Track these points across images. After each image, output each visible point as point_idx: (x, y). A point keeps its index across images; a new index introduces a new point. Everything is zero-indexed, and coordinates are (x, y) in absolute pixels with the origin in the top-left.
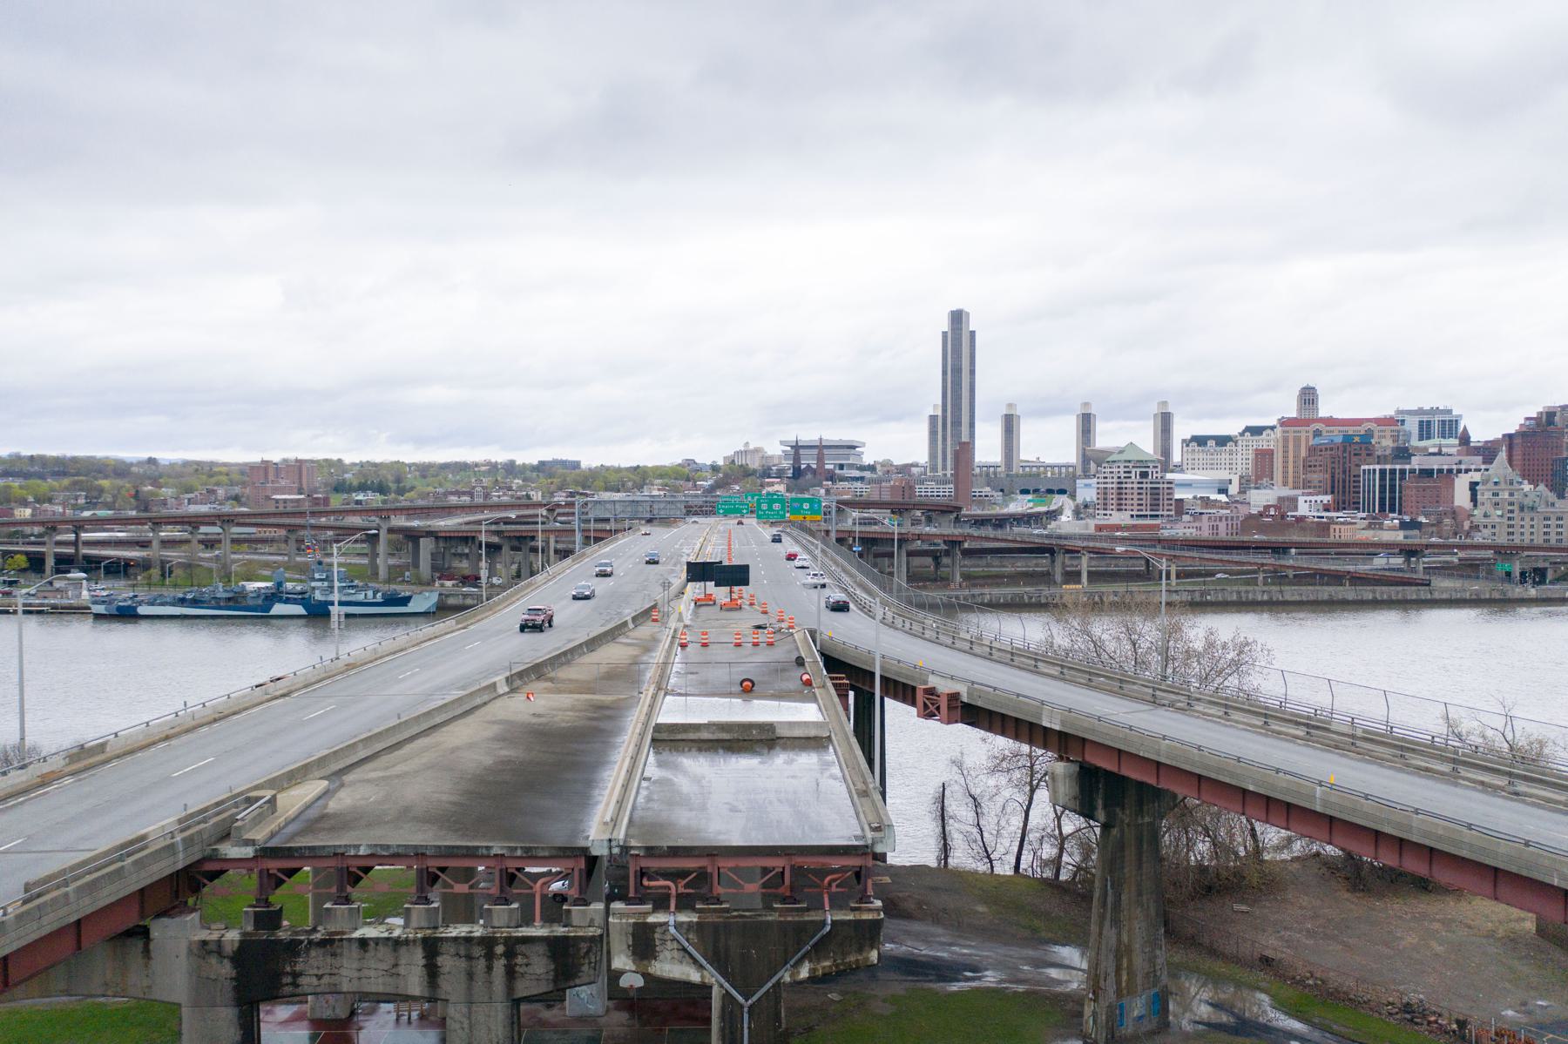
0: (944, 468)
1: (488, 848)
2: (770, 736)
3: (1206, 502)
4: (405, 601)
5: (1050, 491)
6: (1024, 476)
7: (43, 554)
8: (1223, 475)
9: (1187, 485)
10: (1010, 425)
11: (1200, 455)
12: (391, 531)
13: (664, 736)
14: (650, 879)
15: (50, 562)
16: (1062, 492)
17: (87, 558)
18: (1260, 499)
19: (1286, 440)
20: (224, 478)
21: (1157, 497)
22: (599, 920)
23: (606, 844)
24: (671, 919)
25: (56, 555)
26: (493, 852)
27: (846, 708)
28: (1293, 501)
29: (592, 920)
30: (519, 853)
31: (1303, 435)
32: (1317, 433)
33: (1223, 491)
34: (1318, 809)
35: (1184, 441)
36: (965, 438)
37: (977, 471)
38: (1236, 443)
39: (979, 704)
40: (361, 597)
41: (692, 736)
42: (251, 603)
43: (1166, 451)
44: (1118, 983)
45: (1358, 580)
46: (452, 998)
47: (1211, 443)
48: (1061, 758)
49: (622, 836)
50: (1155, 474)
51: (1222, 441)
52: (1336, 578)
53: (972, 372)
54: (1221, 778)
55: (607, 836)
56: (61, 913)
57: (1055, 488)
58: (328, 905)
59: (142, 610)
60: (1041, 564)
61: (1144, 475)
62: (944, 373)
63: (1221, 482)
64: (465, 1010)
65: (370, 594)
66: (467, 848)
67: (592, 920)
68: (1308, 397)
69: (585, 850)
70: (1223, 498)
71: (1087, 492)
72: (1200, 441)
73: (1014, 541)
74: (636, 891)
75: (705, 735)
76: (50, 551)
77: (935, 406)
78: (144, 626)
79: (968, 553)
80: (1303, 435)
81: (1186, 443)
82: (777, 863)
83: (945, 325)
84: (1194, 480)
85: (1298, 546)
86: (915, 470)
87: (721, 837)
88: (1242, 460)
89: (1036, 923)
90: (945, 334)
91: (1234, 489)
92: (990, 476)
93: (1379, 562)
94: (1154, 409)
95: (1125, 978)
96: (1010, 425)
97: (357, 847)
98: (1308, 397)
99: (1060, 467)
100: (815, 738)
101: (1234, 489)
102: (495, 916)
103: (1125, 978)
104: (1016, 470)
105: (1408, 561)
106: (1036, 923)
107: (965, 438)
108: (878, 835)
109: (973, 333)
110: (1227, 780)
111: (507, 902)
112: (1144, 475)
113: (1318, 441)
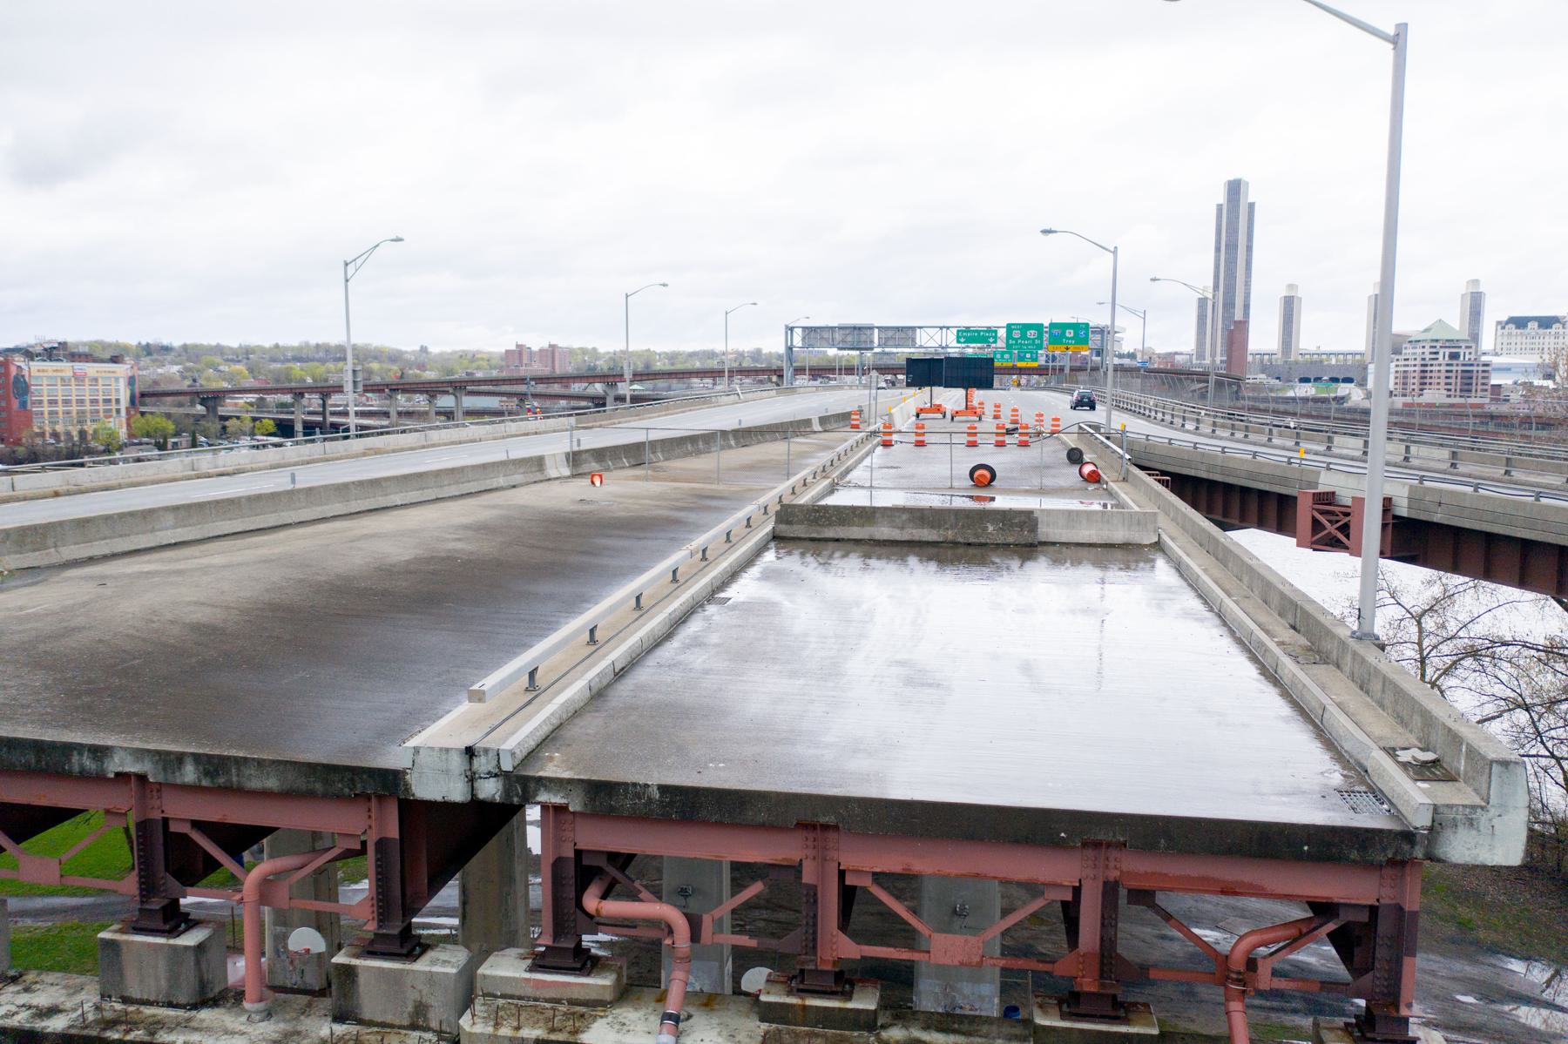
0: (1213, 355)
1: (99, 752)
2: (1026, 536)
3: (1528, 386)
5: (1334, 380)
6: (1306, 363)
7: (292, 421)
9: (1506, 369)
10: (1289, 308)
13: (799, 530)
15: (299, 427)
16: (1349, 380)
20: (485, 364)
21: (1468, 380)
23: (457, 763)
26: (114, 765)
29: (421, 1009)
30: (189, 774)
33: (1549, 376)
35: (1499, 323)
36: (1238, 316)
37: (1250, 358)
39: (1438, 517)
41: (856, 532)
43: (1475, 337)
47: (1533, 325)
50: (1466, 355)
53: (1249, 248)
61: (1454, 356)
62: (1218, 249)
66: (38, 746)
67: (421, 1009)
69: (389, 783)
70: (1550, 384)
72: (1520, 323)
75: (884, 532)
76: (299, 419)
81: (1502, 325)
82: (1059, 870)
83: (1221, 198)
86: (1178, 358)
87: (860, 764)
89: (1464, 912)
90: (1220, 207)
96: (1289, 308)
100: (1125, 546)
102: (128, 959)
106: (1464, 912)
107: (1238, 316)
108: (1446, 794)
109: (1252, 206)
112: (1454, 356)
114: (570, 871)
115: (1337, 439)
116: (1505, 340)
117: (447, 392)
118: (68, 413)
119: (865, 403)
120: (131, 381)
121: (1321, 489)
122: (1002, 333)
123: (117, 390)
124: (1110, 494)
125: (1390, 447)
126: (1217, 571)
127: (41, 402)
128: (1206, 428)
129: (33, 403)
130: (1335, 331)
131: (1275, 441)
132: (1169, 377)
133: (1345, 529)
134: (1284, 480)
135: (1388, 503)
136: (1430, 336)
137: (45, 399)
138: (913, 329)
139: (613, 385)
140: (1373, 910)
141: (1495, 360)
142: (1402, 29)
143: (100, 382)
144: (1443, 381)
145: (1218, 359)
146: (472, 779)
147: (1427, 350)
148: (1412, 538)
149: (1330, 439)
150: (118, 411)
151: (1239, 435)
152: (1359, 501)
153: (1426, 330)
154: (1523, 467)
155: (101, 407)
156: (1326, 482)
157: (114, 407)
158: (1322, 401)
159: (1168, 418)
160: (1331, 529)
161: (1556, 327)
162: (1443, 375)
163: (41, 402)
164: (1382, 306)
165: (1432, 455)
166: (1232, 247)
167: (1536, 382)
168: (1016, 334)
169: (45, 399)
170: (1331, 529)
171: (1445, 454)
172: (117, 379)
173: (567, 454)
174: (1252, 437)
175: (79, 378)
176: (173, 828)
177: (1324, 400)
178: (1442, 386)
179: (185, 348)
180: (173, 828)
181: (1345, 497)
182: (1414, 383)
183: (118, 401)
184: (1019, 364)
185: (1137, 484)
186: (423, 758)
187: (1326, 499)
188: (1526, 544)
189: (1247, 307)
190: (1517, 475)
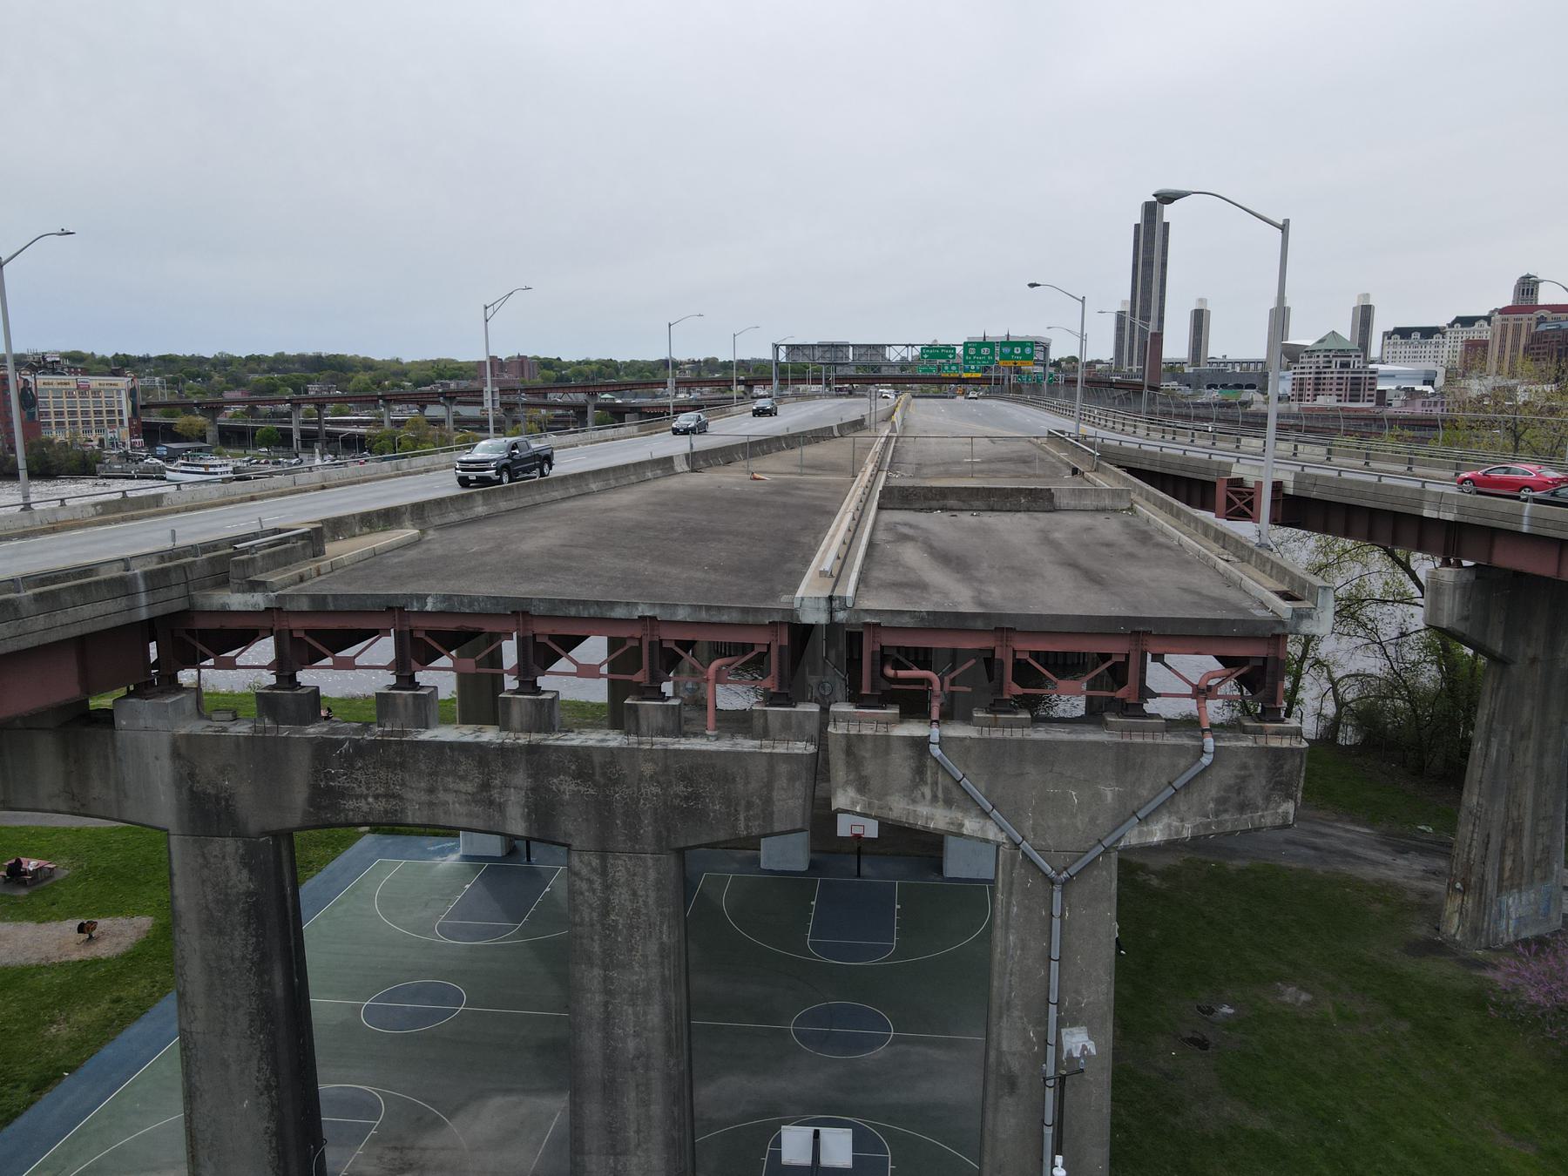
3: (1411, 392)
5: (1239, 386)
8: (1431, 366)
9: (1390, 376)
10: (1199, 319)
11: (1403, 348)
12: (597, 407)
14: (898, 665)
16: (1252, 387)
17: (328, 433)
18: (1475, 386)
19: (1504, 328)
21: (1358, 386)
22: (812, 727)
23: (823, 604)
24: (935, 733)
25: (302, 431)
28: (1511, 391)
31: (1525, 324)
32: (1542, 320)
33: (1431, 383)
35: (1385, 334)
38: (1443, 335)
39: (1314, 494)
43: (1364, 345)
44: (1501, 869)
46: (576, 844)
48: (1446, 563)
49: (850, 592)
50: (1356, 363)
51: (1428, 333)
53: (1164, 265)
55: (827, 594)
57: (1244, 383)
61: (1345, 365)
63: (1427, 372)
64: (595, 862)
68: (1528, 286)
70: (1429, 389)
71: (1282, 384)
72: (1404, 333)
74: (873, 687)
77: (1124, 303)
80: (1525, 324)
81: (1388, 335)
83: (1138, 218)
84: (1396, 372)
86: (1098, 366)
88: (1449, 350)
90: (1137, 226)
91: (1440, 381)
92: (1174, 369)
94: (1355, 302)
95: (1508, 864)
96: (1199, 319)
97: (422, 598)
98: (1528, 286)
99: (1249, 363)
101: (1440, 381)
102: (642, 713)
103: (1508, 864)
104: (1204, 367)
109: (1167, 225)
112: (1345, 365)
113: (1542, 327)
114: (878, 657)
115: (1244, 440)
116: (1391, 349)
117: (438, 403)
118: (75, 423)
119: (866, 412)
120: (132, 393)
121: (1233, 476)
122: (959, 350)
123: (120, 402)
124: (714, 568)
125: (1282, 445)
126: (1174, 521)
127: (47, 414)
128: (1141, 431)
129: (41, 414)
130: (1239, 340)
131: (1198, 442)
132: (1099, 385)
133: (1250, 504)
134: (1207, 471)
135: (1277, 486)
136: (1323, 346)
137: (52, 410)
138: (883, 346)
139: (593, 395)
140: (1265, 659)
141: (1381, 367)
142: (1287, 222)
143: (102, 394)
144: (1334, 387)
145: (1135, 368)
146: (831, 612)
147: (1321, 359)
148: (1296, 509)
149: (1238, 441)
150: (121, 422)
151: (1169, 437)
152: (1259, 484)
153: (1321, 341)
154: (1377, 459)
155: (80, 419)
156: (1237, 471)
157: (117, 418)
158: (1227, 396)
159: (1110, 424)
160: (1240, 504)
161: (1437, 338)
162: (1335, 381)
163: (47, 414)
164: (1280, 318)
165: (1312, 452)
166: (1148, 264)
167: (1418, 388)
168: (972, 351)
169: (52, 410)
170: (1240, 504)
171: (1323, 450)
172: (119, 392)
173: (687, 456)
174: (1178, 439)
175: (83, 390)
176: (665, 645)
177: (1229, 406)
178: (1334, 392)
179: (162, 359)
180: (665, 645)
181: (1250, 481)
182: (1309, 388)
183: (120, 412)
184: (965, 375)
185: (1104, 471)
186: (806, 602)
187: (1239, 482)
188: (1372, 511)
189: (1161, 320)
190: (1373, 465)
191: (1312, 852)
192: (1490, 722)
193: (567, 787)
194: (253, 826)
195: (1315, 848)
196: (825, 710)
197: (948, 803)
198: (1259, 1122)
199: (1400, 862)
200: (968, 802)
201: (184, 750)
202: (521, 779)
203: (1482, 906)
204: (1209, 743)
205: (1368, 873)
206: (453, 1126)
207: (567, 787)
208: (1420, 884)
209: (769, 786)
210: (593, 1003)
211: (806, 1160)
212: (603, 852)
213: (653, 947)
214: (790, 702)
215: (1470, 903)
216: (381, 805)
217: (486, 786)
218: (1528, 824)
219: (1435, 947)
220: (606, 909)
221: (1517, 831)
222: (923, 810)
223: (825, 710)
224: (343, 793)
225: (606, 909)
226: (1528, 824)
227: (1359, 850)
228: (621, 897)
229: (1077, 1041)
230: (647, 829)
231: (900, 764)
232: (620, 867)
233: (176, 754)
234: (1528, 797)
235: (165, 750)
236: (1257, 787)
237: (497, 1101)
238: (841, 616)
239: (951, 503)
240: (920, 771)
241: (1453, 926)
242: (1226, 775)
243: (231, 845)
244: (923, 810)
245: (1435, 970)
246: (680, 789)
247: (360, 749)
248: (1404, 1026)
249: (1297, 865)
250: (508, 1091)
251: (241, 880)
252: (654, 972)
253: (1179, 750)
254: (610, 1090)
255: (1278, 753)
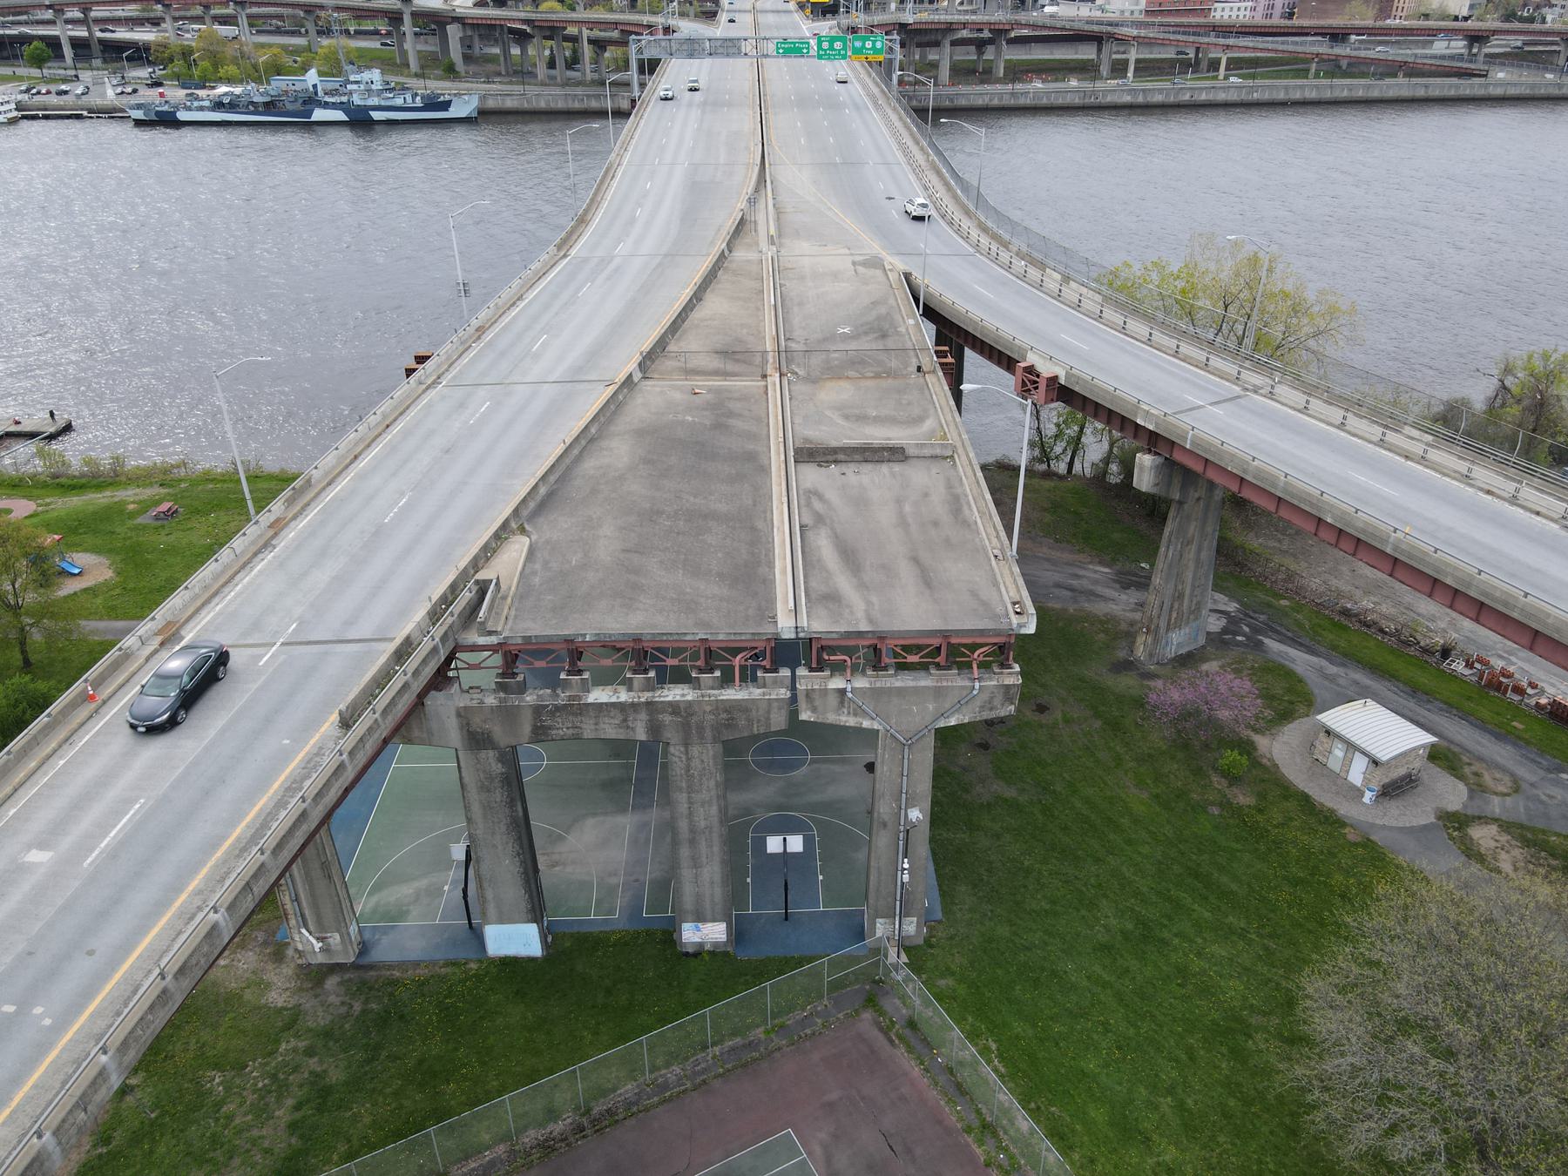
4: (446, 106)
22: (788, 682)
27: (1010, 538)
34: (1389, 550)
39: (1076, 389)
40: (399, 102)
42: (290, 107)
45: (1412, 70)
52: (1391, 69)
54: (1302, 506)
56: (376, 736)
58: (563, 676)
59: (182, 116)
60: (1087, 53)
65: (409, 99)
73: (1063, 29)
78: (187, 135)
79: (1012, 41)
85: (1359, 31)
93: (1440, 47)
95: (1174, 615)
103: (1174, 615)
105: (1470, 47)
110: (1307, 508)
111: (711, 671)
191: (1069, 593)
192: (1171, 533)
193: (667, 718)
194: (502, 744)
195: (1072, 590)
196: (793, 673)
197: (855, 715)
198: (1010, 793)
199: (1124, 597)
200: (865, 714)
201: (463, 715)
202: (643, 716)
203: (1156, 641)
204: (977, 685)
205: (1100, 608)
206: (571, 839)
207: (667, 718)
208: (1130, 615)
209: (769, 712)
210: (683, 808)
211: (781, 850)
212: (686, 745)
213: (712, 783)
214: (776, 671)
215: (1150, 640)
216: (570, 731)
217: (625, 720)
218: (1188, 592)
219: (1127, 666)
220: (688, 768)
221: (1181, 596)
222: (844, 718)
223: (793, 673)
224: (550, 728)
225: (688, 768)
226: (1188, 592)
227: (1099, 589)
228: (696, 763)
229: (915, 814)
230: (708, 734)
231: (833, 701)
232: (695, 750)
233: (459, 715)
234: (1189, 575)
235: (453, 712)
236: (997, 702)
237: (590, 822)
238: (802, 635)
239: (841, 457)
240: (842, 703)
241: (1140, 652)
242: (985, 696)
243: (491, 753)
244: (844, 718)
245: (1126, 683)
246: (724, 716)
247: (557, 708)
248: (1098, 724)
249: (1058, 606)
250: (594, 815)
251: (498, 768)
252: (713, 793)
253: (963, 688)
254: (693, 842)
255: (1008, 687)
